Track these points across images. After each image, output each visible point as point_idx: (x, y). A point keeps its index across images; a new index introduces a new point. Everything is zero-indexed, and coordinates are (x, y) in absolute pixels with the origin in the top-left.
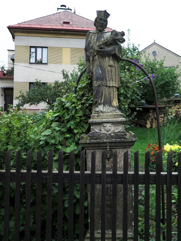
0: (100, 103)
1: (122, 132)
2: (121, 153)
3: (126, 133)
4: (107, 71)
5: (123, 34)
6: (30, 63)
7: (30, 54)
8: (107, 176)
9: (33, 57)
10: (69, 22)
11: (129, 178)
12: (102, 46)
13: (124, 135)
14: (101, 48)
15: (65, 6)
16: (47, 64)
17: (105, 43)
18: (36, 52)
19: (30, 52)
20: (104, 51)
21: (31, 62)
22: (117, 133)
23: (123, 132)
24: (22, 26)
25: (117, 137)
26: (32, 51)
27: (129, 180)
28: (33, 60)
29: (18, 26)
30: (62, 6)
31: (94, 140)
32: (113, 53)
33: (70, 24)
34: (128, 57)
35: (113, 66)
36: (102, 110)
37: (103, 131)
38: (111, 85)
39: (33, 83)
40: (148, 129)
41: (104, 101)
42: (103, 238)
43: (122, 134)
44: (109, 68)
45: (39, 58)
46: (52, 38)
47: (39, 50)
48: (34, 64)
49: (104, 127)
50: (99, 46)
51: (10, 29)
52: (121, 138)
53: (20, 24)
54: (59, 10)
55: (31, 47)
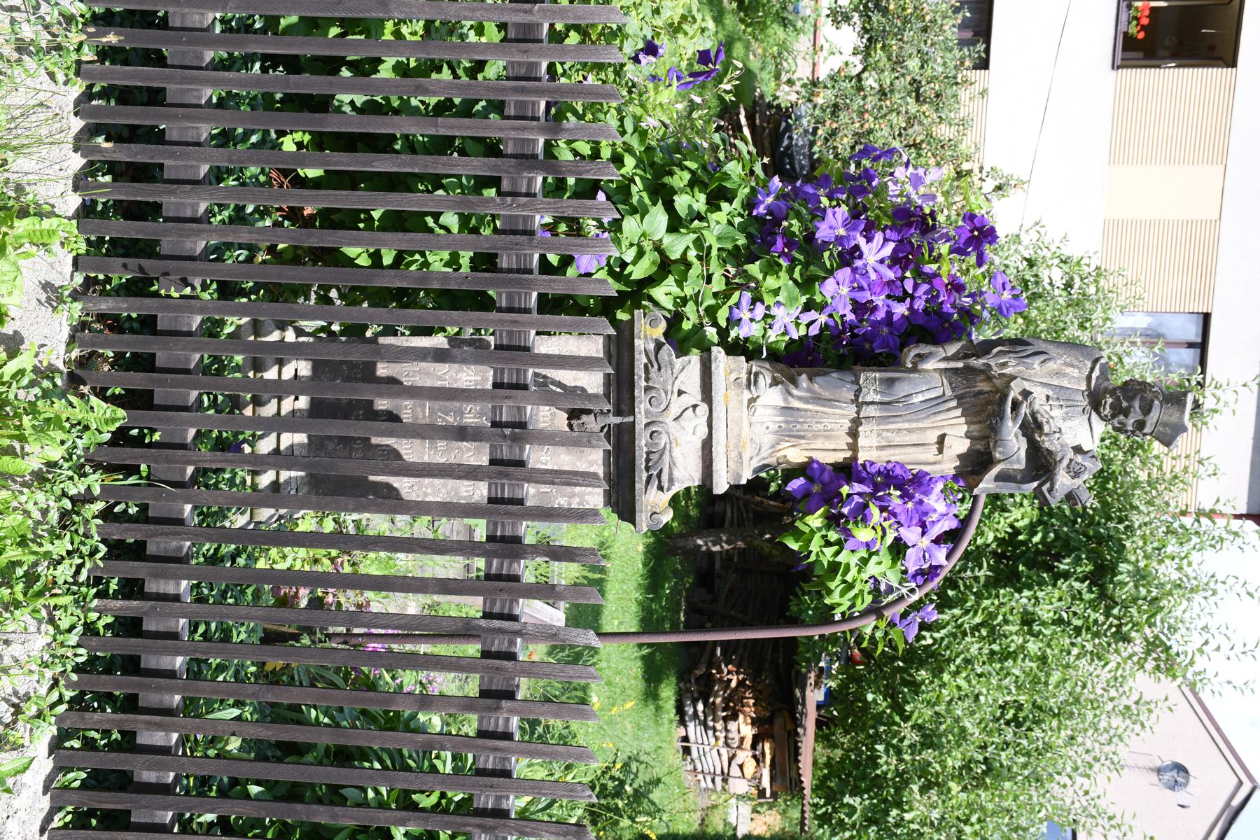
0: (790, 394)
1: (671, 475)
2: (593, 460)
3: (899, 726)
4: (920, 425)
8: (519, 408)
11: (510, 485)
12: (1024, 409)
13: (660, 481)
14: (1016, 406)
17: (1035, 419)
20: (1002, 417)
22: (667, 452)
23: (671, 481)
25: (653, 457)
27: (503, 485)
31: (646, 365)
32: (998, 455)
35: (940, 451)
36: (759, 402)
37: (677, 405)
38: (861, 442)
39: (988, 41)
40: (449, 208)
42: (3, 436)
43: (665, 477)
44: (933, 437)
49: (695, 407)
50: (1026, 394)
52: (647, 468)
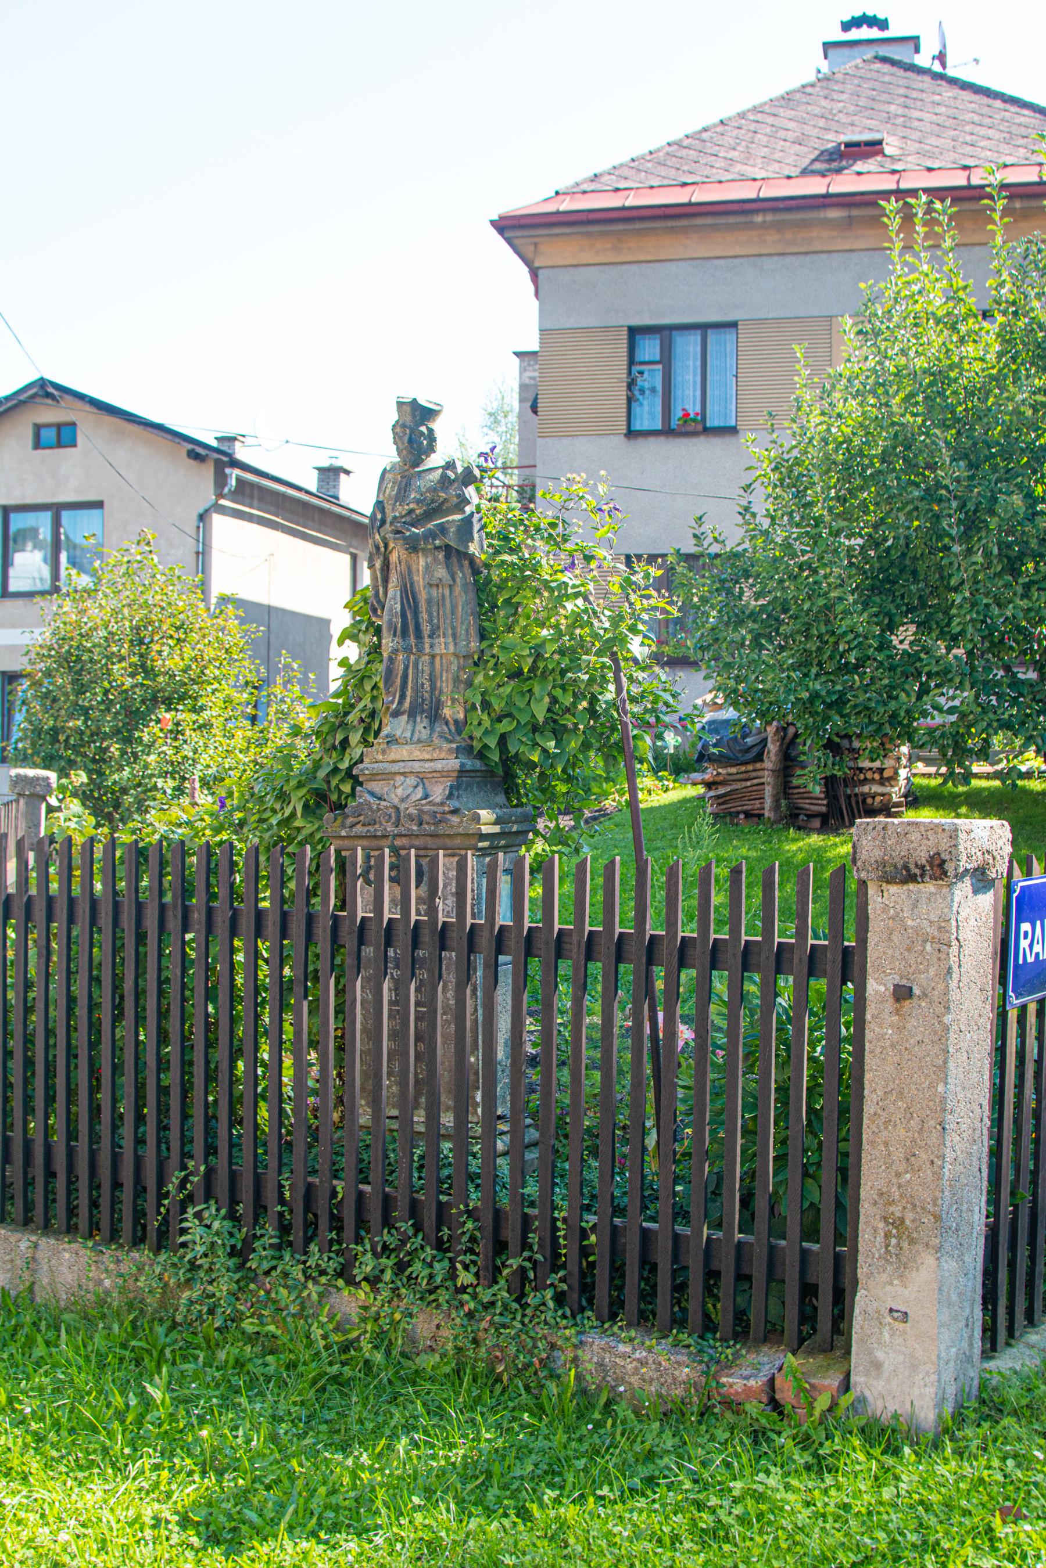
5: (400, 405)
6: (631, 434)
7: (630, 373)
9: (653, 390)
10: (880, 143)
15: (883, 25)
16: (732, 431)
18: (666, 360)
19: (631, 361)
21: (637, 426)
24: (566, 205)
26: (640, 357)
28: (648, 416)
29: (551, 208)
30: (846, 27)
33: (888, 150)
34: (943, 694)
41: (658, 1142)
45: (687, 400)
46: (769, 263)
47: (687, 347)
48: (652, 440)
51: (509, 234)
53: (577, 191)
54: (830, 52)
55: (634, 333)
